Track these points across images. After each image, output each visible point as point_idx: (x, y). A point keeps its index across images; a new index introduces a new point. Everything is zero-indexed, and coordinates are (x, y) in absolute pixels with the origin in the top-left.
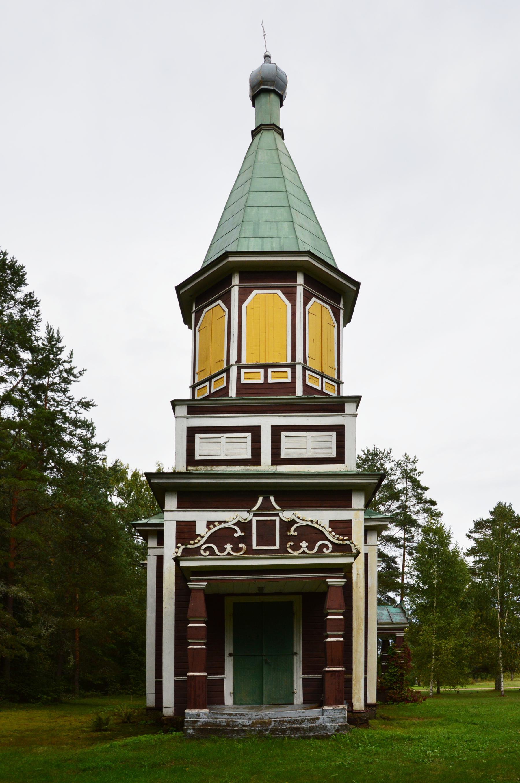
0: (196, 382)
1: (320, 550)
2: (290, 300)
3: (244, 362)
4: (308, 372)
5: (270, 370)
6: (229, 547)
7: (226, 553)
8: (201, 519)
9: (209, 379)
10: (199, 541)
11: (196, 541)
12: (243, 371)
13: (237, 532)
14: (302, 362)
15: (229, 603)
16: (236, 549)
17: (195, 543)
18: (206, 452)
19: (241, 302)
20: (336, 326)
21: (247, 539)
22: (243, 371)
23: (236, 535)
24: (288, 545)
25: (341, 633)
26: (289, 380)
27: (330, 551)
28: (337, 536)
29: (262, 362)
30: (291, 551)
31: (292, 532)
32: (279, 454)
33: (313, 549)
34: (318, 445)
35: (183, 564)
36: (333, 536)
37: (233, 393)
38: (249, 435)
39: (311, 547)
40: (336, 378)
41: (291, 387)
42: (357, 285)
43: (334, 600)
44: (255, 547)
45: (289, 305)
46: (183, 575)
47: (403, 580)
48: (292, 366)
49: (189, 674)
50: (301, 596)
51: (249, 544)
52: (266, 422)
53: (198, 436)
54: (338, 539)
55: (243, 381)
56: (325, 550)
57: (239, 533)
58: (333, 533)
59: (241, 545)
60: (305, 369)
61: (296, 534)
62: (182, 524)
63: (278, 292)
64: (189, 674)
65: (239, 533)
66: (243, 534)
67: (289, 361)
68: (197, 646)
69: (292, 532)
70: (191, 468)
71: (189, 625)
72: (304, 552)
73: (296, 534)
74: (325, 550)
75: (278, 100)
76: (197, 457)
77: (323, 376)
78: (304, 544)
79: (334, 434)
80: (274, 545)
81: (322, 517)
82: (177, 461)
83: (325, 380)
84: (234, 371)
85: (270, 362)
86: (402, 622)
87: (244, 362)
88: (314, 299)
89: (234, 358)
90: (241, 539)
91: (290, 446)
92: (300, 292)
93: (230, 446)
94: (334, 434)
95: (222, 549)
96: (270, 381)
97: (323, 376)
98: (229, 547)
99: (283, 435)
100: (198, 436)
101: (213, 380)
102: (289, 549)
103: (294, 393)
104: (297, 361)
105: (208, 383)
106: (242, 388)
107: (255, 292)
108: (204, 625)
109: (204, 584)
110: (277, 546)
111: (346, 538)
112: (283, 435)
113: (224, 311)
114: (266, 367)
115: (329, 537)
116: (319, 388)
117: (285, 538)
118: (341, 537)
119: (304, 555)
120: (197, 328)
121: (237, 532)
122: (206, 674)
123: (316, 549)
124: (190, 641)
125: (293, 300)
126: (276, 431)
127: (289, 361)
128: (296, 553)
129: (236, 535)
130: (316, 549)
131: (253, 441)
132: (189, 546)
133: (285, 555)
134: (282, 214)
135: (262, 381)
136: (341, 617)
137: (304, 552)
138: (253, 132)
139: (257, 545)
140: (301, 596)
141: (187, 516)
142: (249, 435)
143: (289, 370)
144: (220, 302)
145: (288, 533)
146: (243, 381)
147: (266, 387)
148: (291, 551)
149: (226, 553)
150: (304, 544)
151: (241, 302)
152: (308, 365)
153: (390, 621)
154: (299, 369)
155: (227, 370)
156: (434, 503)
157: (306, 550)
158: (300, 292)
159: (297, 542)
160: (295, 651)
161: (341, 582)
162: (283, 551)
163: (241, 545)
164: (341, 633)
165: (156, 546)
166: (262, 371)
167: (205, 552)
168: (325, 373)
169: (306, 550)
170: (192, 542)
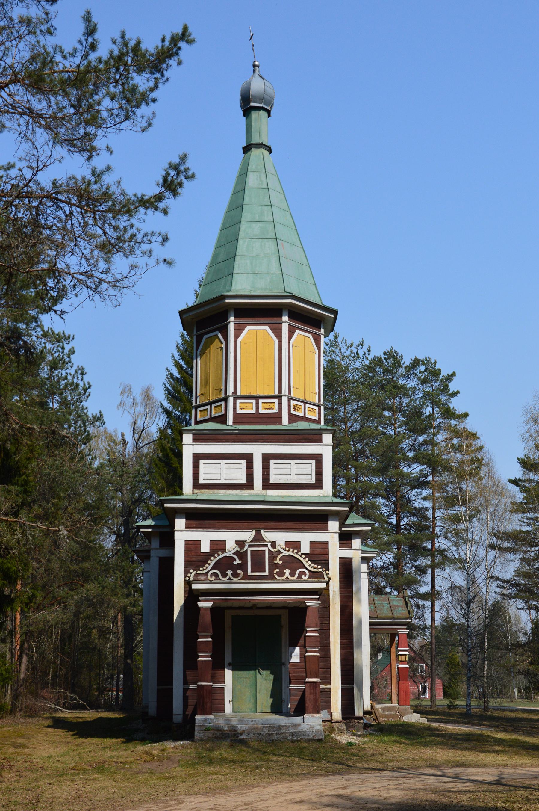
0: (198, 403)
1: (300, 577)
2: (276, 336)
3: (239, 393)
4: (292, 402)
5: (261, 401)
6: (229, 572)
7: (228, 578)
8: (205, 538)
9: (210, 404)
10: (207, 567)
11: (205, 568)
12: (238, 401)
13: (235, 560)
14: (287, 394)
15: (228, 615)
16: (235, 575)
17: (204, 570)
18: (209, 477)
19: (236, 337)
20: (317, 351)
21: (243, 567)
22: (238, 401)
23: (235, 563)
24: (275, 572)
25: (317, 649)
26: (276, 411)
27: (307, 577)
28: (312, 565)
29: (255, 394)
30: (277, 577)
31: (278, 561)
32: (269, 480)
33: (294, 576)
34: (300, 472)
35: (194, 586)
36: (310, 565)
37: (230, 421)
38: (244, 462)
39: (292, 574)
40: (317, 402)
41: (276, 418)
42: (335, 312)
43: (311, 618)
44: (249, 573)
45: (276, 341)
46: (192, 596)
47: (433, 545)
48: (279, 397)
49: (200, 683)
50: (287, 611)
51: (245, 572)
52: (257, 450)
53: (202, 462)
54: (314, 568)
55: (238, 411)
56: (303, 576)
57: (238, 561)
58: (310, 562)
59: (239, 571)
60: (290, 399)
61: (281, 562)
62: (190, 543)
63: (267, 328)
64: (200, 683)
65: (238, 561)
66: (240, 562)
67: (276, 393)
68: (204, 657)
69: (278, 561)
70: (196, 491)
71: (199, 640)
72: (287, 578)
73: (281, 562)
74: (303, 576)
75: (266, 114)
76: (201, 481)
77: (305, 403)
78: (287, 571)
79: (313, 462)
80: (265, 571)
81: (306, 538)
82: (187, 495)
83: (307, 405)
84: (231, 400)
85: (260, 394)
86: (404, 616)
87: (239, 393)
88: (297, 332)
89: (231, 390)
90: (239, 566)
91: (279, 472)
92: (285, 328)
93: (229, 471)
94: (313, 462)
95: (225, 575)
96: (261, 411)
97: (305, 403)
98: (229, 572)
99: (272, 462)
100: (202, 462)
101: (213, 406)
102: (276, 576)
103: (280, 423)
104: (283, 393)
105: (208, 407)
106: (239, 418)
107: (248, 328)
108: (210, 639)
109: (210, 604)
110: (267, 573)
111: (319, 567)
112: (272, 462)
113: (222, 343)
114: (257, 398)
115: (306, 565)
116: (302, 415)
117: (273, 566)
118: (316, 566)
119: (287, 581)
120: (198, 352)
121: (235, 560)
122: (211, 684)
123: (296, 576)
124: (200, 654)
125: (278, 334)
126: (266, 458)
127: (276, 393)
128: (281, 579)
129: (235, 563)
130: (296, 576)
131: (247, 467)
132: (199, 572)
133: (273, 581)
134: (270, 247)
135: (254, 411)
136: (317, 634)
137: (287, 578)
138: (244, 148)
139: (252, 571)
140: (287, 611)
141: (194, 535)
142: (244, 462)
143: (276, 401)
144: (217, 332)
145: (275, 562)
146: (238, 411)
147: (257, 418)
148: (277, 577)
149: (228, 578)
150: (287, 571)
151: (236, 337)
152: (292, 395)
153: (391, 615)
154: (285, 400)
155: (225, 400)
156: (474, 436)
157: (289, 577)
158: (285, 328)
159: (282, 568)
160: (283, 661)
161: (317, 604)
162: (271, 577)
163: (239, 571)
164: (317, 649)
165: (158, 547)
166: (254, 401)
167: (211, 577)
168: (308, 399)
169: (289, 577)
170: (201, 569)
